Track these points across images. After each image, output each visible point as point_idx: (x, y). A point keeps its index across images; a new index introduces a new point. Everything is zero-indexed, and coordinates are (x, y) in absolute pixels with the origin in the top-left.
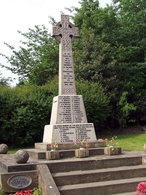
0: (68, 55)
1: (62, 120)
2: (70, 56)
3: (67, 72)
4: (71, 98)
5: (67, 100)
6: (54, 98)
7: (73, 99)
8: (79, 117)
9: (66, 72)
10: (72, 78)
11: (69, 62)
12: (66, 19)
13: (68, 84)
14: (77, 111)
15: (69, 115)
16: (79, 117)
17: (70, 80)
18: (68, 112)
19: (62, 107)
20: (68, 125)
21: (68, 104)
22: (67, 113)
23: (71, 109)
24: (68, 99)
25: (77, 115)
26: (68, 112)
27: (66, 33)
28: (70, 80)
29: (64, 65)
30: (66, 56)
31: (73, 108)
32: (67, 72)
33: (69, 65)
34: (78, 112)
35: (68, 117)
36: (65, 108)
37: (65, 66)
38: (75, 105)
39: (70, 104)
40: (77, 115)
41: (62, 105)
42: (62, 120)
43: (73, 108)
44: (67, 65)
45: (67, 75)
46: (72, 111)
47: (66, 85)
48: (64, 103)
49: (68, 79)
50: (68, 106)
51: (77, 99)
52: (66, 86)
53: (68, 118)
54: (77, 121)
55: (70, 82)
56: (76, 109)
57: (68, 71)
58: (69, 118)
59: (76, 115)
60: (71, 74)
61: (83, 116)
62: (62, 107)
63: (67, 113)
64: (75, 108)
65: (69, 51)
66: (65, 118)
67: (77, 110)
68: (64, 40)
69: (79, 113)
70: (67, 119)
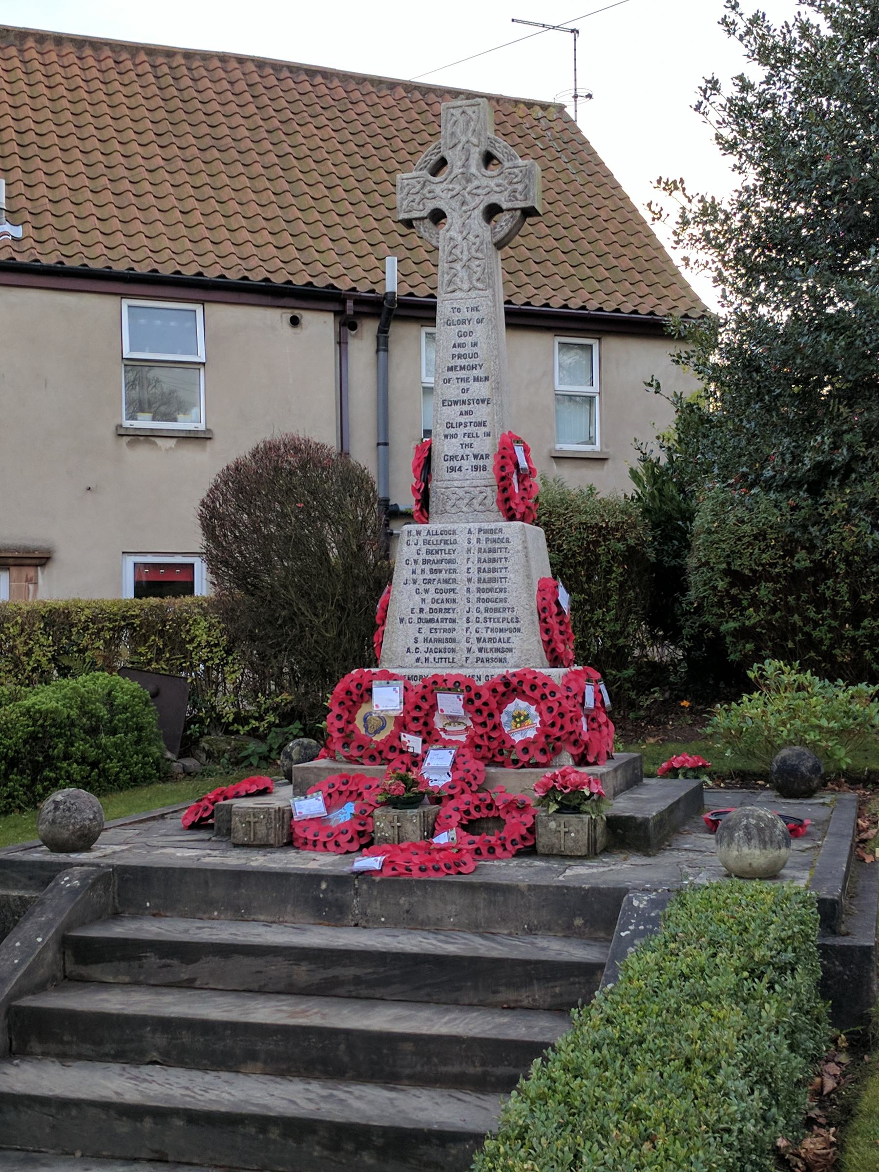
1: (408, 650)
2: (479, 321)
3: (464, 402)
4: (461, 538)
5: (442, 546)
6: (541, 530)
8: (498, 635)
9: (456, 403)
10: (489, 435)
12: (468, 123)
13: (465, 464)
14: (490, 605)
15: (448, 625)
16: (498, 635)
17: (476, 442)
18: (441, 610)
19: (415, 582)
21: (448, 566)
22: (435, 616)
23: (461, 595)
24: (446, 542)
26: (441, 610)
27: (468, 198)
28: (476, 442)
29: (450, 369)
30: (464, 322)
31: (468, 590)
32: (464, 402)
34: (497, 610)
35: (438, 635)
36: (428, 586)
37: (451, 374)
39: (455, 571)
40: (488, 624)
41: (414, 572)
42: (408, 650)
43: (468, 590)
44: (462, 368)
45: (463, 419)
46: (461, 606)
47: (453, 469)
48: (425, 562)
49: (467, 440)
50: (446, 581)
51: (494, 541)
52: (455, 475)
53: (439, 641)
54: (483, 655)
55: (475, 457)
56: (485, 596)
57: (465, 397)
58: (448, 640)
59: (482, 625)
61: (519, 630)
62: (415, 582)
63: (435, 616)
64: (479, 590)
65: (473, 294)
66: (425, 640)
67: (487, 600)
69: (497, 615)
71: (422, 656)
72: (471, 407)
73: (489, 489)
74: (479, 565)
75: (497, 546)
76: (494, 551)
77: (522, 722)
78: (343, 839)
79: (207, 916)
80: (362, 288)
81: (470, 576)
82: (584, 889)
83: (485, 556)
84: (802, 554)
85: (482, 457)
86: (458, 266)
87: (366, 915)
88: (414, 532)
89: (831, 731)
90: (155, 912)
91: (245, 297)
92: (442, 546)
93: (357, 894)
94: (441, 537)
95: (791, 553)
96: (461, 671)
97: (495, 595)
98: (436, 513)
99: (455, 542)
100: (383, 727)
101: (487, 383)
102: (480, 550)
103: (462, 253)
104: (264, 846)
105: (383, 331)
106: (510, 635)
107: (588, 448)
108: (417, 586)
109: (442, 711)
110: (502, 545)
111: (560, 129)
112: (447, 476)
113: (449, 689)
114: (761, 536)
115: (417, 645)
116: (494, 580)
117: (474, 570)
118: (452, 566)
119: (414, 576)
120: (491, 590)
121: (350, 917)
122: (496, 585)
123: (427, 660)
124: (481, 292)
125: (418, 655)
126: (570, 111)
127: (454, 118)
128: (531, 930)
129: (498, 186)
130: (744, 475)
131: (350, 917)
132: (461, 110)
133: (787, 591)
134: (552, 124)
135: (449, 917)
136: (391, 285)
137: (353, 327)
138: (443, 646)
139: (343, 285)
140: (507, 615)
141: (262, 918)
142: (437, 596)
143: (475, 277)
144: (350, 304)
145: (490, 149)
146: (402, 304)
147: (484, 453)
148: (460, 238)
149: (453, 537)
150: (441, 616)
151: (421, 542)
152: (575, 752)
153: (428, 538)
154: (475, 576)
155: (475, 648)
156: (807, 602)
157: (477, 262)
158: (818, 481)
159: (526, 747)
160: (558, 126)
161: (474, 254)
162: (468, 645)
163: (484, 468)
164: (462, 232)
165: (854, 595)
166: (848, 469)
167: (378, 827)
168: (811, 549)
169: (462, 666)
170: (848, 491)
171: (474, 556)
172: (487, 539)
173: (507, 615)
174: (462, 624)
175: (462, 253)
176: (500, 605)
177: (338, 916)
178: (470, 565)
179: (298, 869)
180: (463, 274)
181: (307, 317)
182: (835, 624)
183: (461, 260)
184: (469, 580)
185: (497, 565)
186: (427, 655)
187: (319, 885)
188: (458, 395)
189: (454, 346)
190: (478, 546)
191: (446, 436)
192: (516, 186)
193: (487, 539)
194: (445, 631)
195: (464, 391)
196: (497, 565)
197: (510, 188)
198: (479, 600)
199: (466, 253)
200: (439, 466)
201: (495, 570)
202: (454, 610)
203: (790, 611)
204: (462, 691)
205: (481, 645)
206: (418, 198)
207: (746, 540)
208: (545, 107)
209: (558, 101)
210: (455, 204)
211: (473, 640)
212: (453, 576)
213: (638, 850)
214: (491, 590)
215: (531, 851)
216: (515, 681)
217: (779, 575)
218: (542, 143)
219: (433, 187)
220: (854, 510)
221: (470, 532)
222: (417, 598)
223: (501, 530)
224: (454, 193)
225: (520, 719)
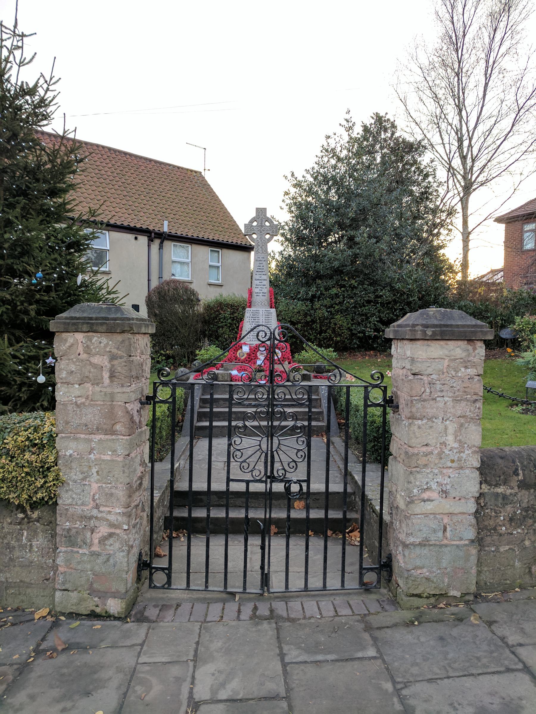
4: (261, 312)
60: (265, 283)
80: (156, 229)
84: (309, 317)
91: (122, 230)
95: (306, 317)
105: (162, 243)
114: (299, 312)
126: (203, 174)
130: (292, 297)
133: (304, 326)
136: (166, 229)
137: (152, 241)
139: (151, 228)
144: (153, 234)
146: (169, 235)
158: (312, 299)
165: (320, 327)
166: (319, 297)
168: (311, 316)
181: (139, 237)
200: (254, 295)
203: (304, 331)
208: (196, 172)
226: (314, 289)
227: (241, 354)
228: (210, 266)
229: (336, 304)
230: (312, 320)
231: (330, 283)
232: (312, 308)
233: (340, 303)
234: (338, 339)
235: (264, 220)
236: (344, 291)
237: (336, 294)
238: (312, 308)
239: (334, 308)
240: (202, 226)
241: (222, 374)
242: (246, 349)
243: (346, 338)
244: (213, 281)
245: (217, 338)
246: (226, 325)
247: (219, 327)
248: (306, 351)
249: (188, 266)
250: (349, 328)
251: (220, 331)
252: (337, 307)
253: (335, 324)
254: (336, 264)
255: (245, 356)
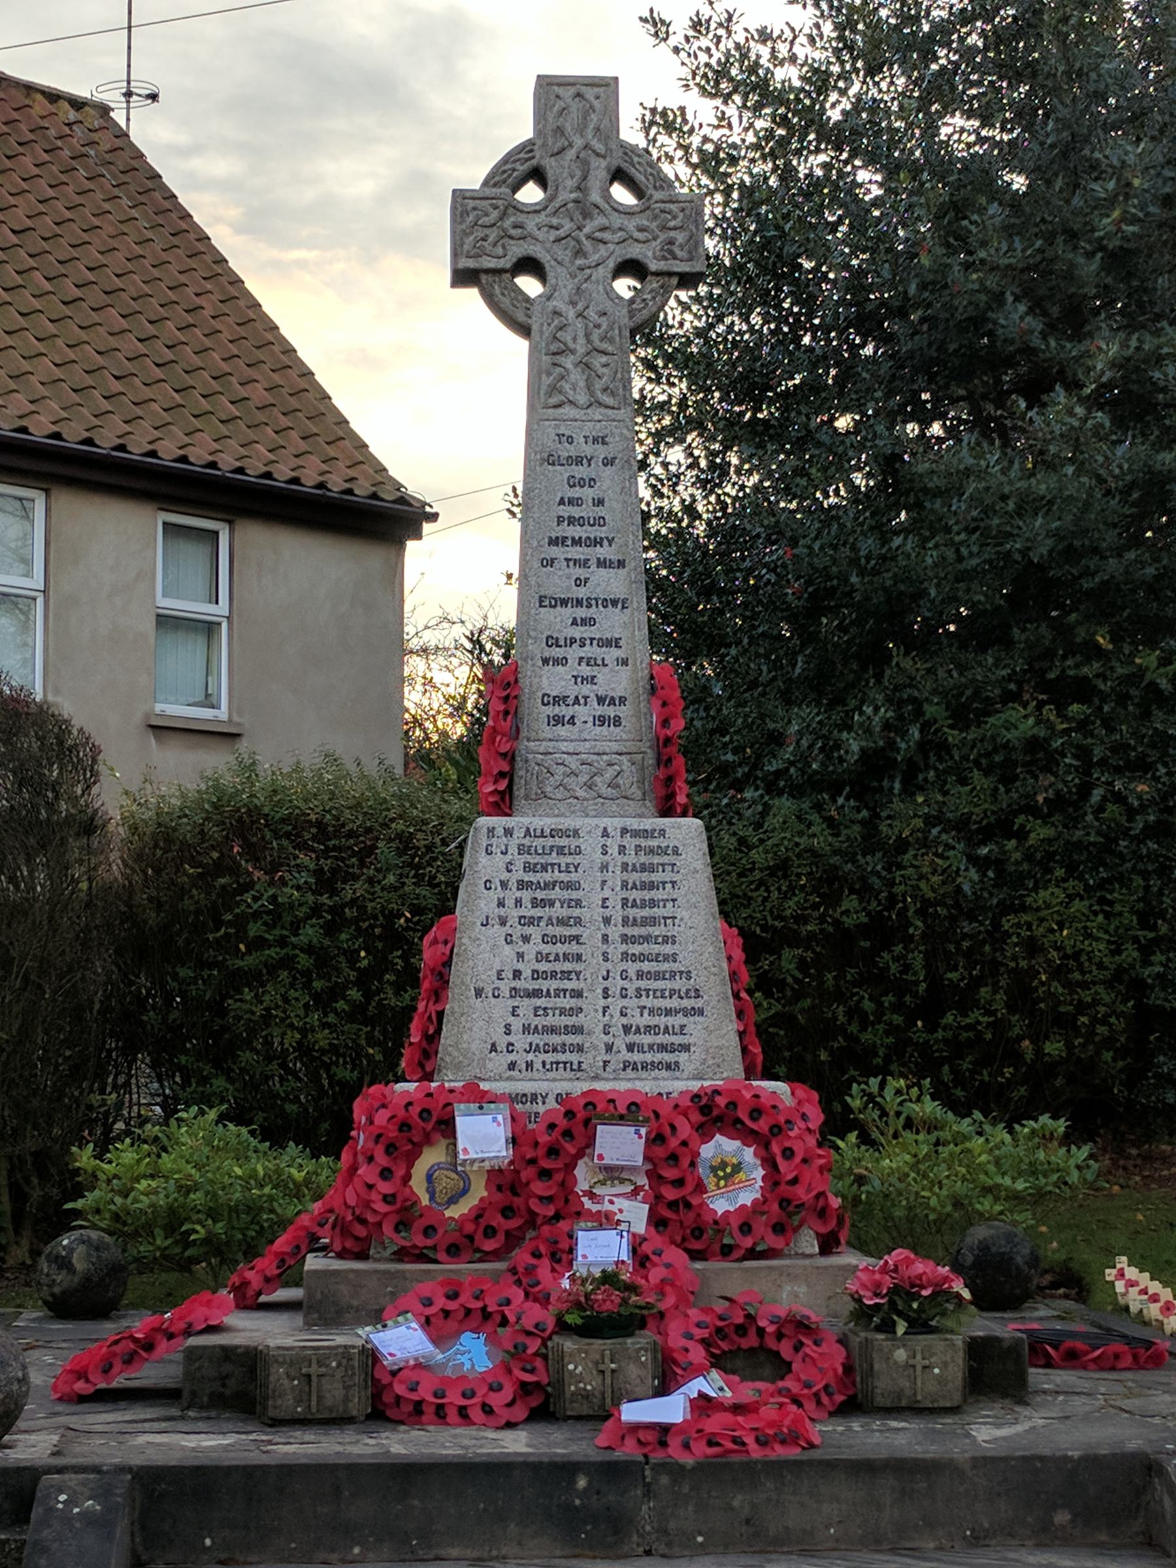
0: (588, 450)
1: (494, 1048)
2: (608, 462)
3: (579, 603)
4: (590, 844)
5: (554, 858)
7: (614, 850)
8: (662, 1021)
9: (564, 602)
10: (625, 662)
11: (600, 511)
14: (646, 966)
15: (567, 1002)
16: (662, 1021)
17: (602, 675)
18: (553, 975)
19: (503, 922)
20: (534, 1097)
21: (566, 894)
22: (544, 985)
23: (591, 945)
24: (561, 851)
25: (648, 1002)
26: (553, 975)
27: (587, 245)
28: (602, 675)
29: (554, 542)
30: (579, 461)
31: (605, 938)
32: (579, 603)
33: (597, 542)
34: (659, 976)
35: (550, 1020)
36: (529, 930)
37: (556, 552)
38: (632, 912)
39: (578, 903)
40: (644, 1001)
41: (501, 904)
42: (494, 1048)
43: (605, 938)
44: (577, 542)
45: (578, 632)
46: (593, 966)
47: (558, 720)
48: (522, 885)
49: (585, 670)
50: (562, 922)
52: (563, 731)
53: (553, 1030)
54: (636, 1057)
56: (636, 949)
57: (581, 593)
58: (568, 1030)
60: (611, 622)
61: (701, 1012)
62: (503, 922)
63: (544, 985)
64: (625, 939)
65: (597, 413)
66: (526, 1029)
67: (642, 957)
68: (556, 313)
69: (660, 984)
70: (536, 1039)
71: (521, 1058)
72: (592, 612)
73: (623, 758)
74: (625, 894)
75: (656, 860)
76: (652, 869)
77: (733, 1172)
78: (497, 1400)
79: (334, 1557)
81: (607, 912)
82: (1071, 1459)
83: (635, 877)
84: (850, 902)
85: (612, 702)
86: (568, 362)
87: (665, 1532)
88: (500, 831)
89: (1016, 1198)
90: (223, 1556)
92: (554, 858)
93: (648, 1493)
94: (550, 842)
95: (833, 900)
96: (599, 1086)
97: (656, 949)
98: (527, 797)
99: (578, 851)
100: (465, 1192)
101: (621, 571)
102: (625, 867)
103: (574, 339)
104: (338, 1421)
106: (684, 1021)
107: (206, 713)
108: (507, 929)
109: (601, 1157)
110: (665, 859)
111: (108, 147)
112: (547, 732)
113: (622, 1117)
114: (781, 868)
115: (510, 1039)
116: (653, 921)
117: (615, 902)
118: (575, 895)
119: (502, 911)
120: (646, 939)
121: (635, 1538)
122: (656, 931)
123: (529, 1065)
124: (610, 412)
125: (512, 1057)
126: (119, 116)
127: (560, 104)
128: (976, 1538)
129: (641, 229)
130: (725, 769)
131: (635, 1538)
132: (572, 90)
134: (95, 137)
135: (827, 1528)
138: (559, 1042)
140: (679, 984)
141: (455, 1552)
142: (546, 949)
143: (598, 385)
145: (625, 166)
147: (617, 694)
148: (571, 314)
149: (574, 842)
150: (554, 985)
151: (513, 850)
152: (824, 1230)
153: (527, 842)
154: (617, 914)
155: (620, 1043)
156: (855, 984)
157: (604, 359)
159: (746, 1220)
160: (106, 142)
161: (597, 343)
162: (606, 1038)
163: (617, 721)
164: (573, 303)
167: (571, 1373)
168: (863, 890)
169: (596, 1078)
170: (920, 799)
171: (615, 878)
172: (638, 848)
173: (679, 984)
174: (593, 1001)
175: (574, 339)
176: (665, 966)
177: (610, 1539)
178: (607, 893)
179: (432, 1455)
180: (577, 376)
182: (898, 1019)
183: (573, 352)
184: (607, 921)
185: (658, 895)
186: (530, 1057)
187: (572, 1482)
188: (569, 589)
189: (561, 502)
190: (620, 859)
191: (545, 661)
192: (672, 234)
193: (638, 848)
194: (563, 1012)
195: (579, 582)
196: (658, 895)
197: (663, 236)
198: (625, 956)
199: (582, 340)
200: (536, 714)
201: (653, 903)
202: (578, 974)
204: (647, 1120)
205: (632, 1038)
206: (493, 235)
207: (757, 875)
208: (78, 104)
209: (100, 97)
210: (564, 254)
211: (617, 1030)
212: (576, 912)
213: (1005, 1395)
214: (646, 939)
215: (853, 1405)
216: (721, 1101)
217: (811, 936)
218: (86, 168)
219: (521, 218)
220: (935, 831)
221: (605, 833)
222: (508, 951)
223: (662, 833)
224: (562, 233)
225: (728, 1172)
226: (875, 713)
227: (447, 1181)
228: (166, 622)
229: (1032, 810)
230: (877, 919)
231: (991, 669)
232: (871, 840)
233: (1058, 803)
234: (1054, 1048)
235: (600, 169)
236: (1083, 725)
237: (1033, 744)
238: (871, 840)
239: (1022, 835)
240: (117, 386)
241: (296, 1360)
242: (483, 1137)
243: (1108, 1042)
244: (176, 710)
245: (221, 1054)
246: (287, 963)
247: (236, 980)
248: (866, 1139)
249: (26, 626)
250: (1119, 974)
251: (246, 1004)
252: (1040, 832)
253: (1032, 947)
254: (1038, 535)
255: (479, 1192)
